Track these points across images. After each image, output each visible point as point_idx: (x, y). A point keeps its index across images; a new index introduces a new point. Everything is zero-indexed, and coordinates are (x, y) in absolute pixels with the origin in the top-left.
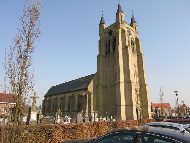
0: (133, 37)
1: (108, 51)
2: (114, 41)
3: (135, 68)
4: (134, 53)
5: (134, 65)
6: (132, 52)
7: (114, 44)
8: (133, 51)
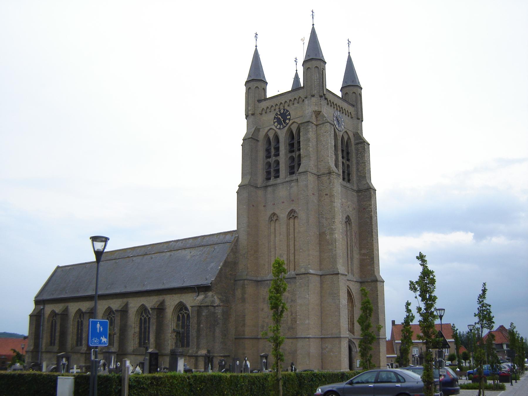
0: (349, 133)
1: (272, 172)
2: (292, 145)
3: (348, 228)
4: (349, 181)
5: (348, 221)
6: (344, 179)
7: (293, 154)
8: (346, 177)
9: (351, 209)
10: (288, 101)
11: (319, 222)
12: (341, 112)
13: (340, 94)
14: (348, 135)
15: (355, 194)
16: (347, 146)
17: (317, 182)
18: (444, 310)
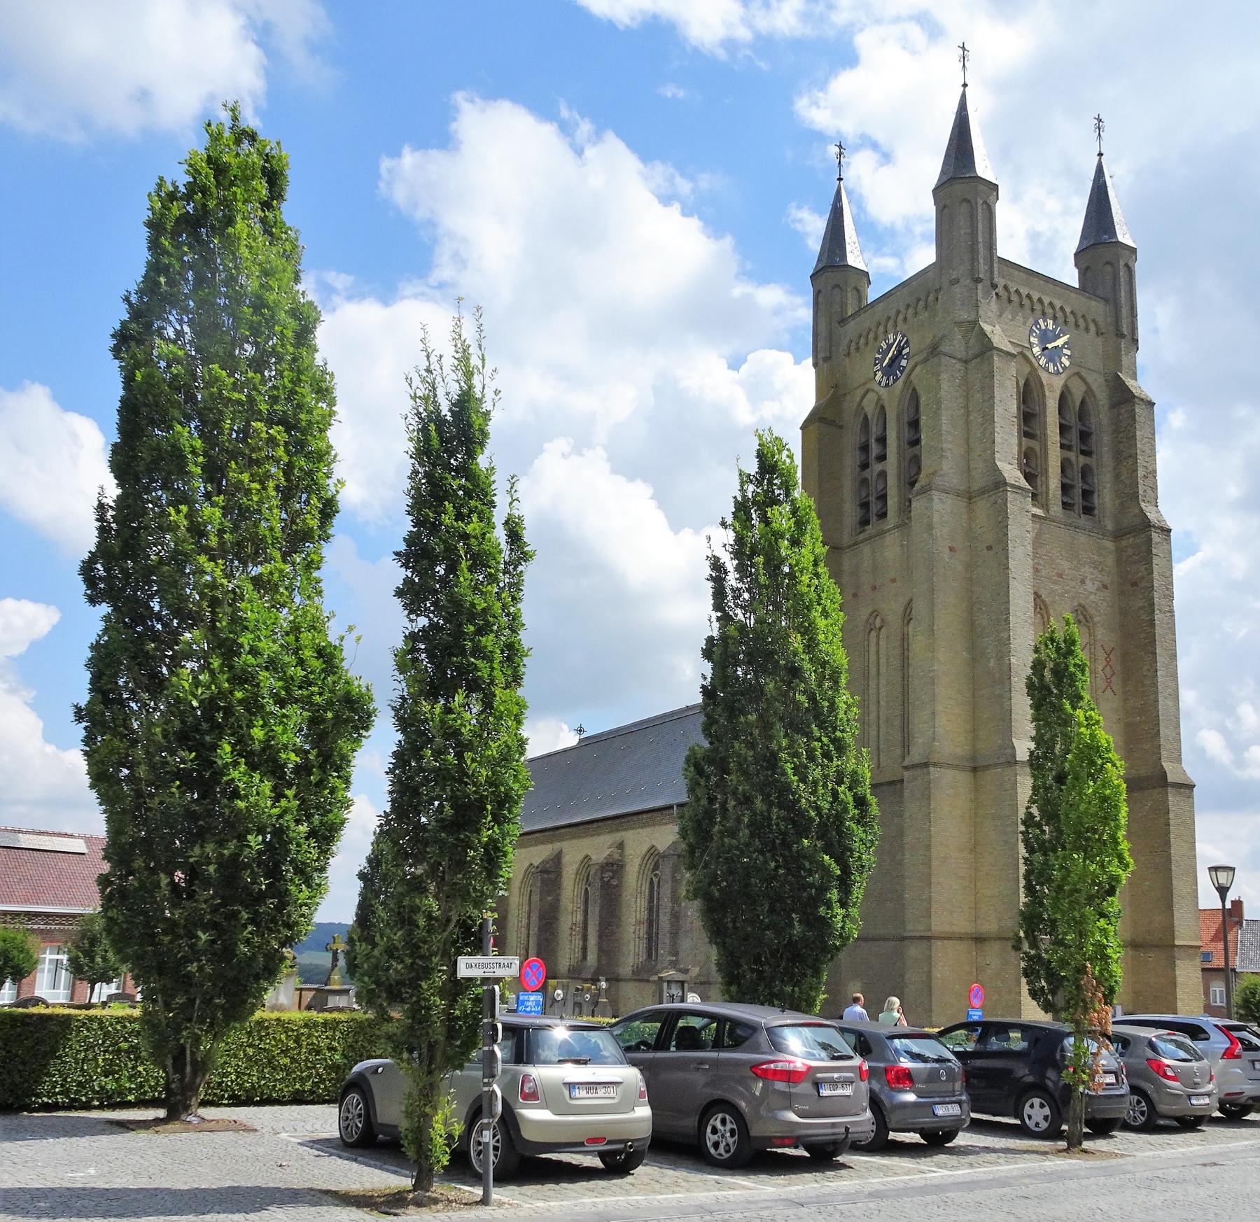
4: (1088, 510)
9: (1090, 586)
10: (902, 309)
11: (972, 623)
12: (1061, 320)
13: (1070, 276)
14: (1086, 383)
15: (1109, 545)
16: (1083, 414)
17: (965, 517)
18: (1233, 869)
